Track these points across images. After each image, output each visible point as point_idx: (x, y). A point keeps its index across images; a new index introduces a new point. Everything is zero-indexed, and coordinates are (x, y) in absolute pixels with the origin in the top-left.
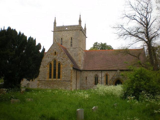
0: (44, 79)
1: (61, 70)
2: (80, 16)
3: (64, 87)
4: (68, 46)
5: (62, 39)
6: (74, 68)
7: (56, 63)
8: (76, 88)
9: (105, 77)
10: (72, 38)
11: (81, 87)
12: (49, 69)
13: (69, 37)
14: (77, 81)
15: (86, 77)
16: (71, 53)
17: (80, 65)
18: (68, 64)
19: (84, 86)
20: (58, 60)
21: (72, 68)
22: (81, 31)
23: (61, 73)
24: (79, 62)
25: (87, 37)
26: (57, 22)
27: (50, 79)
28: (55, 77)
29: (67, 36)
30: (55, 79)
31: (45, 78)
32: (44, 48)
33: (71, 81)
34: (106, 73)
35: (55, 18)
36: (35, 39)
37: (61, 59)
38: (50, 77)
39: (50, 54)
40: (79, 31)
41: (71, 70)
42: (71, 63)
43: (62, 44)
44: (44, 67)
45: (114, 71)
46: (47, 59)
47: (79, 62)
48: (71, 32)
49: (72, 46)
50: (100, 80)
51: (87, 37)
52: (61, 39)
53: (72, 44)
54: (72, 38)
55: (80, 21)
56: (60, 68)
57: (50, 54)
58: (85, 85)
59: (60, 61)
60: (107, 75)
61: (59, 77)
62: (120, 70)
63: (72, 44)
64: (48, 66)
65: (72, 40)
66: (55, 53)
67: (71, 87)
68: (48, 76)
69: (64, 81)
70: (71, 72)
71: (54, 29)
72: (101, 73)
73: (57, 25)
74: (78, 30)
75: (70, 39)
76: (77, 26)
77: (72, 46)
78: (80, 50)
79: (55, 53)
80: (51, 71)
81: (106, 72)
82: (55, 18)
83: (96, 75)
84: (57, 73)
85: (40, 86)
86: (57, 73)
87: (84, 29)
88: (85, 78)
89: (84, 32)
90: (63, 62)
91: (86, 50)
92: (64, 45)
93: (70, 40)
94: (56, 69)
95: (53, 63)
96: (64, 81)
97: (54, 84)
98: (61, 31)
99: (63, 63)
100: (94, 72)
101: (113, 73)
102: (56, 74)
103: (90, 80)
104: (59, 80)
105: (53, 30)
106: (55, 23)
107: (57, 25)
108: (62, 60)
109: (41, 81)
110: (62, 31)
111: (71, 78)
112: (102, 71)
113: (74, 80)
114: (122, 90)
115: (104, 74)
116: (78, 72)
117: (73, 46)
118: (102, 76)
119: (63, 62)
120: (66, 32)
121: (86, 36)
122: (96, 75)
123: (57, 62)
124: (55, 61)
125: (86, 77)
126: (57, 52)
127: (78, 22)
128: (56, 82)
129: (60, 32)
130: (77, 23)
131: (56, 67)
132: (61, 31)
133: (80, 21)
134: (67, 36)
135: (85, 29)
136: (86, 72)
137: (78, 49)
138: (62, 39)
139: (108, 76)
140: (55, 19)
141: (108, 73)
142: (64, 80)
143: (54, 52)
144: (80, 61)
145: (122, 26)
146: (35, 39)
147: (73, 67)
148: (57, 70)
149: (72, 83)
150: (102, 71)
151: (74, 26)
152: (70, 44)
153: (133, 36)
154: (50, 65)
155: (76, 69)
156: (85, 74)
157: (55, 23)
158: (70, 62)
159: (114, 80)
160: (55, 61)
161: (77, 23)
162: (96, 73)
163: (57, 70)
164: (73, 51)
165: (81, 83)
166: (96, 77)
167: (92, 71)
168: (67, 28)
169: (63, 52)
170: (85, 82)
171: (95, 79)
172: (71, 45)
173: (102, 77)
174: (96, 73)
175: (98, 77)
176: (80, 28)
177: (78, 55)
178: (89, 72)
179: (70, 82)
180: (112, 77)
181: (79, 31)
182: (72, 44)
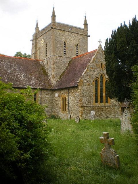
0: (89, 105)
28: (102, 101)
30: (102, 104)
46: (92, 72)
54: (77, 45)
55: (86, 24)
104: (107, 104)
120: (70, 33)
138: (65, 43)
152: (76, 53)
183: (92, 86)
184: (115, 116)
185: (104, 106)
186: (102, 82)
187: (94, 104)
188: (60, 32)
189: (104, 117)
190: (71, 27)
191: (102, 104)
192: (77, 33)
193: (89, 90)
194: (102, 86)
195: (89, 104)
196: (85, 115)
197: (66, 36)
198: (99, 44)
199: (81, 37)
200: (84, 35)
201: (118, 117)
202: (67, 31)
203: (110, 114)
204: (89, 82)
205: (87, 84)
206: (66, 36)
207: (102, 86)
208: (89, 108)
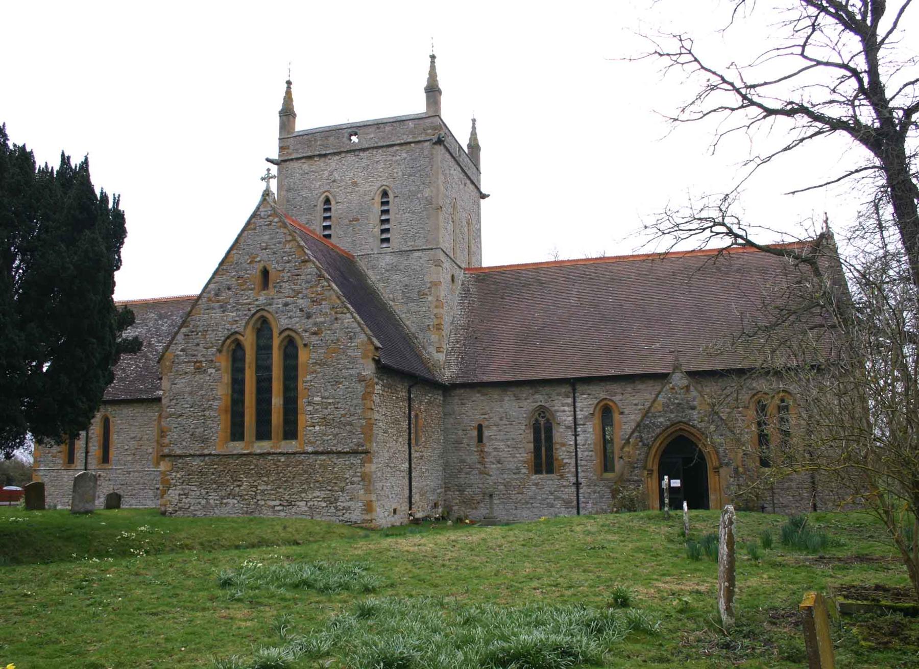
0: (196, 448)
1: (305, 379)
2: (433, 62)
3: (323, 494)
4: (359, 242)
5: (327, 201)
6: (383, 369)
7: (271, 338)
8: (410, 497)
9: (597, 420)
10: (385, 194)
11: (447, 489)
12: (227, 378)
13: (372, 188)
14: (414, 455)
15: (480, 428)
16: (380, 286)
17: (441, 357)
18: (344, 339)
19: (471, 486)
20: (284, 322)
21: (369, 370)
22: (440, 149)
23: (302, 402)
24: (434, 338)
25: (484, 196)
26: (297, 107)
27: (238, 447)
28: (263, 433)
29: (354, 184)
30: (264, 446)
31: (204, 440)
32: (121, 208)
33: (367, 452)
34: (602, 396)
35: (289, 83)
36: (86, 162)
37: (301, 310)
38: (237, 433)
39: (233, 282)
40: (425, 153)
41: (361, 379)
42: (363, 337)
43: (327, 233)
44: (199, 369)
45: (651, 383)
46: (217, 315)
47: (434, 338)
48: (379, 155)
49: (387, 240)
50: (563, 445)
51: (484, 196)
52: (321, 206)
53: (387, 230)
54: (385, 194)
55: (433, 91)
56: (295, 368)
57: (233, 282)
58: (474, 478)
59: (297, 323)
60: (606, 413)
61: (291, 432)
62: (691, 374)
63: (387, 226)
64: (224, 362)
65: (387, 203)
66: (265, 273)
67: (368, 491)
68: (220, 426)
69: (322, 453)
70: (366, 396)
71: (281, 148)
72: (570, 401)
73: (302, 124)
74: (420, 146)
75: (378, 199)
76: (417, 119)
77: (387, 240)
78: (438, 264)
79: (265, 273)
80: (242, 392)
81: (600, 393)
82: (289, 83)
83: (542, 411)
84: (277, 401)
85: (173, 495)
86: (277, 401)
87: (466, 151)
88: (475, 433)
89: (465, 160)
90: (315, 333)
91: (484, 265)
92: (342, 241)
93: (378, 208)
94: (270, 380)
95: (249, 341)
96: (322, 453)
97: (260, 475)
98: (321, 156)
99: (314, 339)
100: (525, 392)
101: (644, 395)
102: (269, 412)
103: (501, 445)
104: (292, 446)
105: (275, 156)
106: (287, 114)
107: (302, 124)
108: (309, 317)
109: (180, 456)
110: (325, 155)
111: (368, 429)
112: (580, 388)
113: (388, 448)
114: (536, 645)
115: (586, 403)
116: (425, 402)
117: (395, 244)
118: (580, 415)
119: (315, 333)
120: (351, 158)
121: (478, 189)
122: (542, 411)
123: (275, 333)
124: (263, 327)
125: (480, 428)
126: (273, 267)
127: (423, 96)
128: (269, 462)
129: (321, 163)
130: (418, 106)
131: (269, 368)
132: (321, 156)
133: (433, 91)
134: (355, 184)
135: (474, 147)
136: (477, 397)
137: (425, 256)
138: (327, 201)
139: (616, 416)
140: (289, 88)
141: (616, 399)
142: (321, 449)
143: (255, 271)
144: (439, 327)
145: (687, 44)
146: (85, 165)
147: (377, 362)
148: (277, 386)
149: (371, 468)
150: (574, 384)
151: (400, 122)
152: (377, 230)
153: (773, 116)
154: (234, 351)
155: (403, 370)
156: (473, 409)
157: (287, 114)
158: (358, 329)
159: (647, 436)
160: (263, 327)
161: (418, 106)
162: (540, 398)
163: (277, 386)
164: (394, 268)
165: (446, 465)
166: (542, 421)
167: (516, 390)
168: (354, 139)
169: (310, 269)
170: (475, 457)
171: (537, 440)
172: (384, 236)
173: (575, 424)
174: (537, 396)
175: (554, 426)
176: (435, 128)
177: (422, 294)
178: (495, 394)
179: (356, 460)
180: (639, 418)
181: (425, 153)
182: (387, 230)
183: (210, 371)
184: (332, 501)
185: (269, 454)
186: (263, 349)
187: (220, 444)
188: (306, 167)
189: (272, 503)
190: (355, 129)
191: (261, 448)
192: (380, 144)
193: (201, 388)
194: (263, 369)
195: (197, 446)
196: (177, 492)
197: (331, 173)
198: (263, 186)
199: (405, 155)
200: (419, 142)
201: (347, 509)
202: (335, 154)
203: (304, 491)
204: (200, 358)
205: (191, 368)
206: (331, 173)
207: (263, 369)
208: (196, 462)
